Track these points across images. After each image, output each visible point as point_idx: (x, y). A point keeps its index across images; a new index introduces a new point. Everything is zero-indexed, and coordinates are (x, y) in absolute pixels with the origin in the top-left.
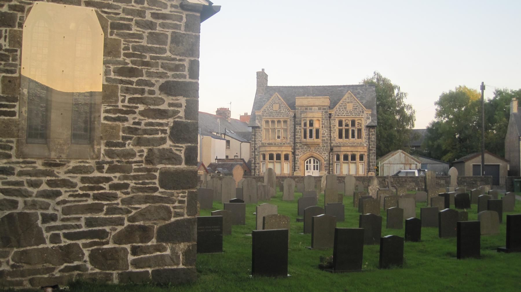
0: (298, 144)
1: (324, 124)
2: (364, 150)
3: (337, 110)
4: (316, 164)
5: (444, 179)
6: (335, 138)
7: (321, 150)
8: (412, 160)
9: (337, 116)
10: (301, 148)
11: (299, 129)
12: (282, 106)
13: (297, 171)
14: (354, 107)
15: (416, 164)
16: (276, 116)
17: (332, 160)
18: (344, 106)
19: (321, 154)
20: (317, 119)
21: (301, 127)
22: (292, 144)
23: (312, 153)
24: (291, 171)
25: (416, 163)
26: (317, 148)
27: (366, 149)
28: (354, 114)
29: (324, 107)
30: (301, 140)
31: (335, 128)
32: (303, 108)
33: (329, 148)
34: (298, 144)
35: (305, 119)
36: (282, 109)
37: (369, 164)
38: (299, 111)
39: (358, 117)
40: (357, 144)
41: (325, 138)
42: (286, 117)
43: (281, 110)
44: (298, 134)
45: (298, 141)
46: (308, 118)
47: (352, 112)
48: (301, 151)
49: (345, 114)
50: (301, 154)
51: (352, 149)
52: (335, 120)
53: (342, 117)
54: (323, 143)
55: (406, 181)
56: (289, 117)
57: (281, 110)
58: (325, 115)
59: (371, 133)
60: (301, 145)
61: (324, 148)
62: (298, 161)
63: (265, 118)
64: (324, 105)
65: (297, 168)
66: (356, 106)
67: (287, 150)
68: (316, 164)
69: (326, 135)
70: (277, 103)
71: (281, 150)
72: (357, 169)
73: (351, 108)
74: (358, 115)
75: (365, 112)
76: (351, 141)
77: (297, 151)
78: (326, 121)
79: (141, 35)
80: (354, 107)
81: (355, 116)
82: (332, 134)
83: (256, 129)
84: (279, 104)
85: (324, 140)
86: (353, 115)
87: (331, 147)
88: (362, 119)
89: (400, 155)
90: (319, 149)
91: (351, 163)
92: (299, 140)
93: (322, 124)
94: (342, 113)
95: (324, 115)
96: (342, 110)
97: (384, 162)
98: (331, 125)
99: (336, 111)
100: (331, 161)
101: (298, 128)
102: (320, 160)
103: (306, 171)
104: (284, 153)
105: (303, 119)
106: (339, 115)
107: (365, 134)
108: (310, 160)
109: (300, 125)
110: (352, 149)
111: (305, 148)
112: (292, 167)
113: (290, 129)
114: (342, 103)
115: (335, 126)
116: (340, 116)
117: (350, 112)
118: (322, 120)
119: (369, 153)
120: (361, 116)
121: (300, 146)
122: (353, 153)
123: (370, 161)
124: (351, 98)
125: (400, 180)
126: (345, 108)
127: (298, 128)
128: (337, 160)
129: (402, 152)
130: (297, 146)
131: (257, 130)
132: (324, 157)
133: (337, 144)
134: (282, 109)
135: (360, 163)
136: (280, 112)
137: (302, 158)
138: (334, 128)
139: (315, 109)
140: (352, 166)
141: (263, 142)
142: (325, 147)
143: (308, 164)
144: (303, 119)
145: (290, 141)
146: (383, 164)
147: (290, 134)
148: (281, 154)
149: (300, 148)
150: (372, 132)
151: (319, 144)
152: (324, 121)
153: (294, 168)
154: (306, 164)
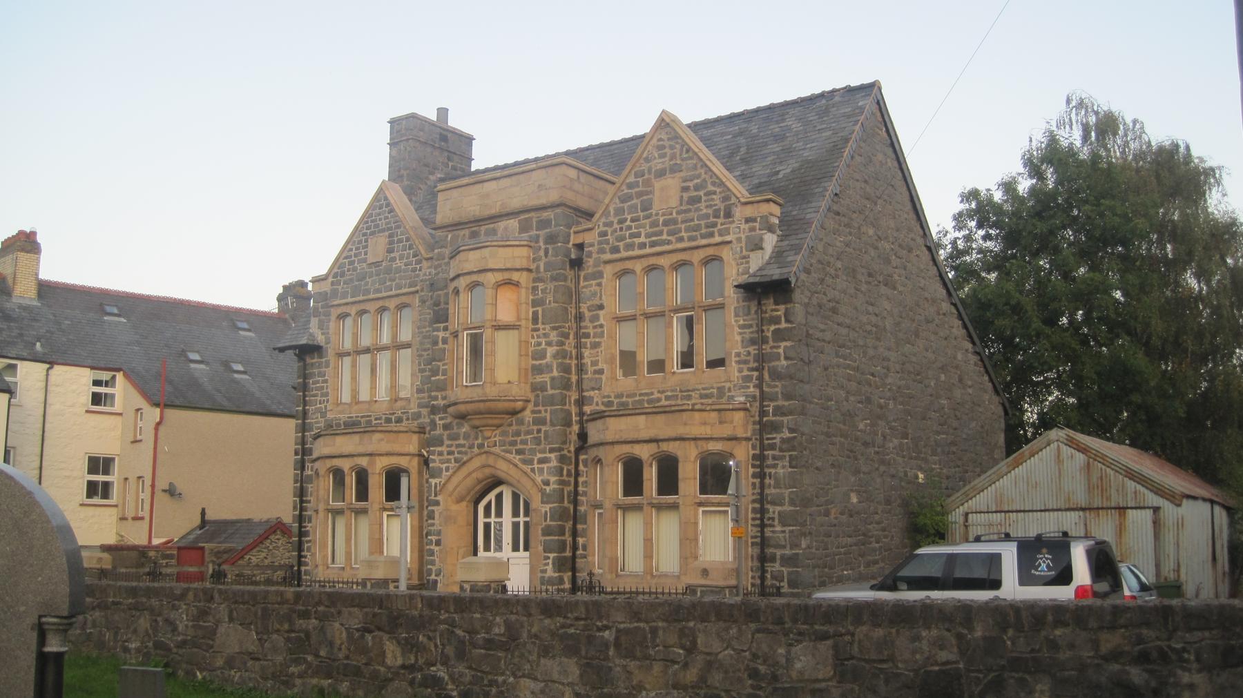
2: (726, 431)
4: (522, 519)
5: (824, 637)
6: (601, 372)
8: (1131, 485)
9: (608, 256)
14: (685, 195)
15: (1156, 510)
18: (640, 195)
19: (525, 462)
23: (491, 461)
25: (1153, 499)
27: (739, 424)
28: (687, 230)
31: (602, 321)
32: (462, 233)
37: (763, 511)
39: (704, 242)
40: (702, 397)
41: (546, 378)
47: (675, 222)
48: (449, 453)
49: (642, 239)
50: (447, 469)
51: (660, 427)
52: (600, 275)
53: (631, 253)
54: (536, 405)
55: (511, 640)
56: (418, 288)
59: (773, 328)
60: (449, 420)
61: (539, 431)
62: (437, 503)
63: (339, 305)
66: (697, 188)
67: (397, 448)
68: (522, 519)
69: (549, 359)
72: (689, 540)
73: (674, 202)
74: (703, 237)
75: (738, 212)
76: (672, 381)
80: (685, 195)
81: (691, 239)
82: (586, 353)
83: (309, 360)
85: (543, 388)
86: (681, 239)
88: (726, 253)
89: (1058, 458)
91: (660, 507)
95: (542, 253)
96: (633, 220)
97: (972, 504)
104: (382, 463)
107: (738, 338)
108: (499, 497)
110: (660, 427)
111: (466, 437)
115: (601, 307)
116: (624, 254)
117: (666, 223)
119: (763, 448)
120: (721, 235)
122: (665, 447)
123: (771, 491)
124: (672, 147)
125: (472, 632)
126: (646, 207)
128: (661, 492)
129: (1071, 443)
131: (312, 364)
132: (539, 479)
135: (700, 504)
136: (388, 271)
137: (450, 487)
139: (506, 228)
140: (668, 528)
141: (330, 416)
145: (420, 406)
146: (967, 515)
148: (370, 471)
150: (776, 320)
152: (541, 286)
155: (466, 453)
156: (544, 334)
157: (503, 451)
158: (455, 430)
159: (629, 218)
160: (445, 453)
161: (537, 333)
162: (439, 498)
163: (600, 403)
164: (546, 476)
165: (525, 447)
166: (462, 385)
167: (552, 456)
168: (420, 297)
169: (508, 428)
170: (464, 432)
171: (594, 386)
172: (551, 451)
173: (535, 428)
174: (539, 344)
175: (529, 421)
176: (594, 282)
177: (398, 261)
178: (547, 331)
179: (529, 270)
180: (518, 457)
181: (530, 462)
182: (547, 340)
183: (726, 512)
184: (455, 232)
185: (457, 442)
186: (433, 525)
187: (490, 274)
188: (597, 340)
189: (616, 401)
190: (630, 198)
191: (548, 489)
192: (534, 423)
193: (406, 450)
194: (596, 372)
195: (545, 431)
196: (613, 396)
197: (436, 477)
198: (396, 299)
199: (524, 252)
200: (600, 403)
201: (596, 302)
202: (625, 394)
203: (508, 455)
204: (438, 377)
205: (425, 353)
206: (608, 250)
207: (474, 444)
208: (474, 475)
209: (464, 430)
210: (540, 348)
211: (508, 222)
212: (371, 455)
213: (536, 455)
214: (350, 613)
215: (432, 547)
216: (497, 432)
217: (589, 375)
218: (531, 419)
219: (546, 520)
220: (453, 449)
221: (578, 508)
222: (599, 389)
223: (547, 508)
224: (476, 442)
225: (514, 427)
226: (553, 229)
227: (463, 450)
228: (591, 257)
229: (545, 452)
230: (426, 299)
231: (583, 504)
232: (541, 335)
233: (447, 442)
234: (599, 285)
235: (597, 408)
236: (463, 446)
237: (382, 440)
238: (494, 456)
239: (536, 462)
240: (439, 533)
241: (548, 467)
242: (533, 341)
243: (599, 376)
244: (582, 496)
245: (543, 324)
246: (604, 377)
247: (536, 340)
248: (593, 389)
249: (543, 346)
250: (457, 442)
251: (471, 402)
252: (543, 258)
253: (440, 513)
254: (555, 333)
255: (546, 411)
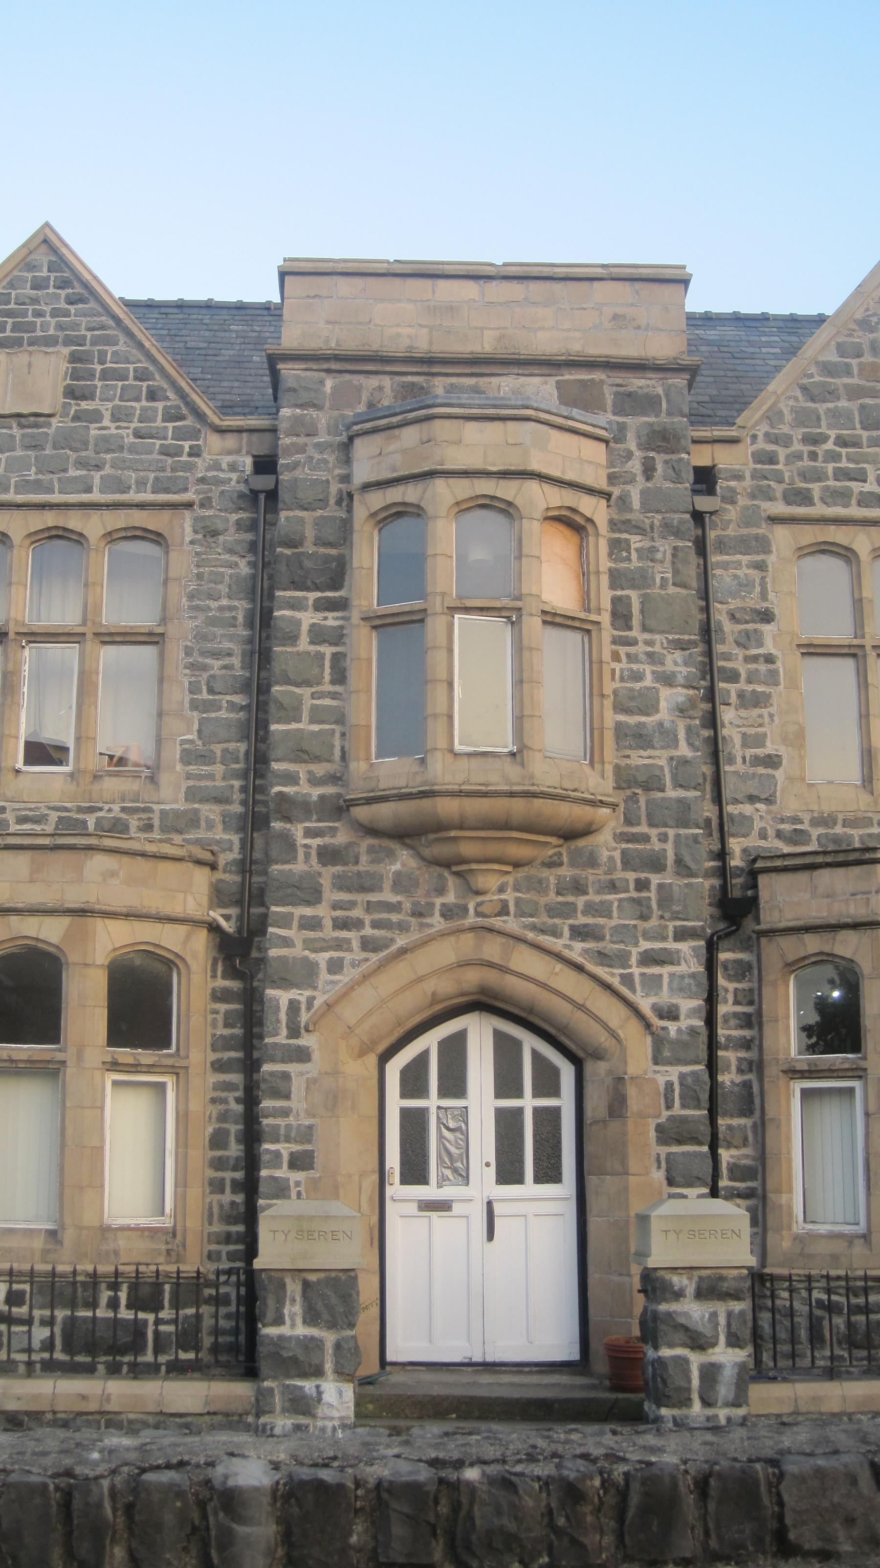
0: (298, 831)
1: (640, 580)
3: (786, 441)
4: (528, 1103)
6: (772, 762)
7: (603, 910)
9: (780, 508)
10: (341, 883)
11: (318, 635)
12: (106, 375)
13: (281, 1190)
16: (25, 486)
17: (746, 1044)
19: (603, 958)
20: (557, 498)
21: (340, 605)
22: (219, 834)
23: (492, 949)
24: (196, 1193)
26: (551, 877)
29: (638, 383)
30: (334, 779)
32: (373, 382)
33: (707, 884)
34: (298, 831)
35: (410, 493)
36: (106, 409)
38: (322, 419)
42: (148, 496)
43: (95, 416)
44: (308, 703)
45: (86, 1434)
46: (440, 484)
48: (342, 924)
52: (763, 545)
56: (189, 496)
57: (95, 416)
58: (649, 470)
60: (342, 838)
62: (302, 1055)
64: (630, 350)
65: (285, 1149)
68: (528, 1103)
69: (664, 714)
70: (50, 341)
71: (74, 897)
77: (285, 921)
78: (664, 547)
79: (822, 1340)
82: (727, 715)
84: (66, 351)
85: (652, 783)
87: (723, 872)
90: (579, 888)
92: (320, 769)
93: (616, 579)
94: (842, 474)
95: (635, 466)
96: (842, 442)
98: (720, 614)
99: (762, 444)
100: (729, 1056)
101: (307, 618)
102: (602, 1038)
103: (395, 1189)
105: (377, 500)
106: (805, 498)
109: (336, 582)
111: (400, 884)
112: (218, 1141)
113: (201, 637)
114: (832, 356)
115: (767, 617)
116: (819, 509)
118: (613, 525)
121: (329, 856)
127: (307, 618)
130: (290, 845)
132: (645, 1004)
133: (798, 836)
134: (106, 409)
137: (349, 1013)
138: (746, 640)
142: (656, 864)
143: (432, 1102)
144: (377, 500)
145: (192, 795)
147: (195, 705)
148: (73, 956)
149: (327, 874)
151: (587, 831)
152: (636, 541)
153: (235, 1150)
154: (395, 1103)
155: (403, 927)
156: (650, 655)
157: (534, 928)
158: (364, 865)
159: (833, 434)
160: (328, 923)
161: (632, 650)
162: (306, 1040)
163: (771, 832)
164: (665, 997)
165: (601, 921)
166: (451, 751)
167: (684, 947)
168: (196, 520)
169: (545, 873)
170: (397, 874)
171: (755, 793)
172: (681, 935)
173: (631, 876)
174: (638, 677)
175: (611, 859)
176: (745, 559)
177: (106, 422)
178: (657, 648)
179: (608, 496)
180: (579, 946)
181: (622, 959)
182: (659, 668)
183: (851, 1091)
184: (348, 377)
185: (374, 897)
186: (285, 1113)
187: (533, 486)
188: (760, 689)
189: (815, 832)
190: (832, 394)
191: (672, 1028)
192: (628, 862)
193: (176, 909)
194: (757, 761)
195: (661, 886)
196: (806, 818)
197: (298, 986)
198: (107, 514)
199: (596, 452)
200: (771, 832)
201: (753, 601)
202: (841, 817)
203: (546, 940)
204: (294, 726)
205: (216, 664)
206: (779, 495)
207: (431, 905)
208: (430, 986)
209: (397, 867)
210: (638, 686)
211: (522, 379)
212: (82, 912)
213: (636, 944)
214: (697, 1454)
215: (278, 1173)
216: (510, 879)
217: (738, 766)
218: (617, 855)
219: (669, 1107)
220: (357, 913)
221: (720, 1078)
222: (769, 801)
223: (673, 1073)
224: (439, 901)
225: (566, 872)
226: (664, 418)
227: (395, 917)
228: (733, 502)
229: (664, 939)
230: (220, 526)
231: (728, 1068)
232: (642, 657)
233: (331, 895)
234: (761, 566)
235: (762, 843)
236: (395, 908)
237: (113, 874)
238: (500, 940)
239: (634, 960)
240: (306, 1135)
241: (672, 976)
242: (617, 666)
243: (770, 771)
244: (726, 1048)
245: (645, 629)
246: (779, 774)
247: (624, 664)
248: (752, 799)
249: (648, 681)
250: (374, 897)
251: (485, 795)
252: (640, 478)
253: (311, 1083)
254: (678, 655)
255: (663, 838)
